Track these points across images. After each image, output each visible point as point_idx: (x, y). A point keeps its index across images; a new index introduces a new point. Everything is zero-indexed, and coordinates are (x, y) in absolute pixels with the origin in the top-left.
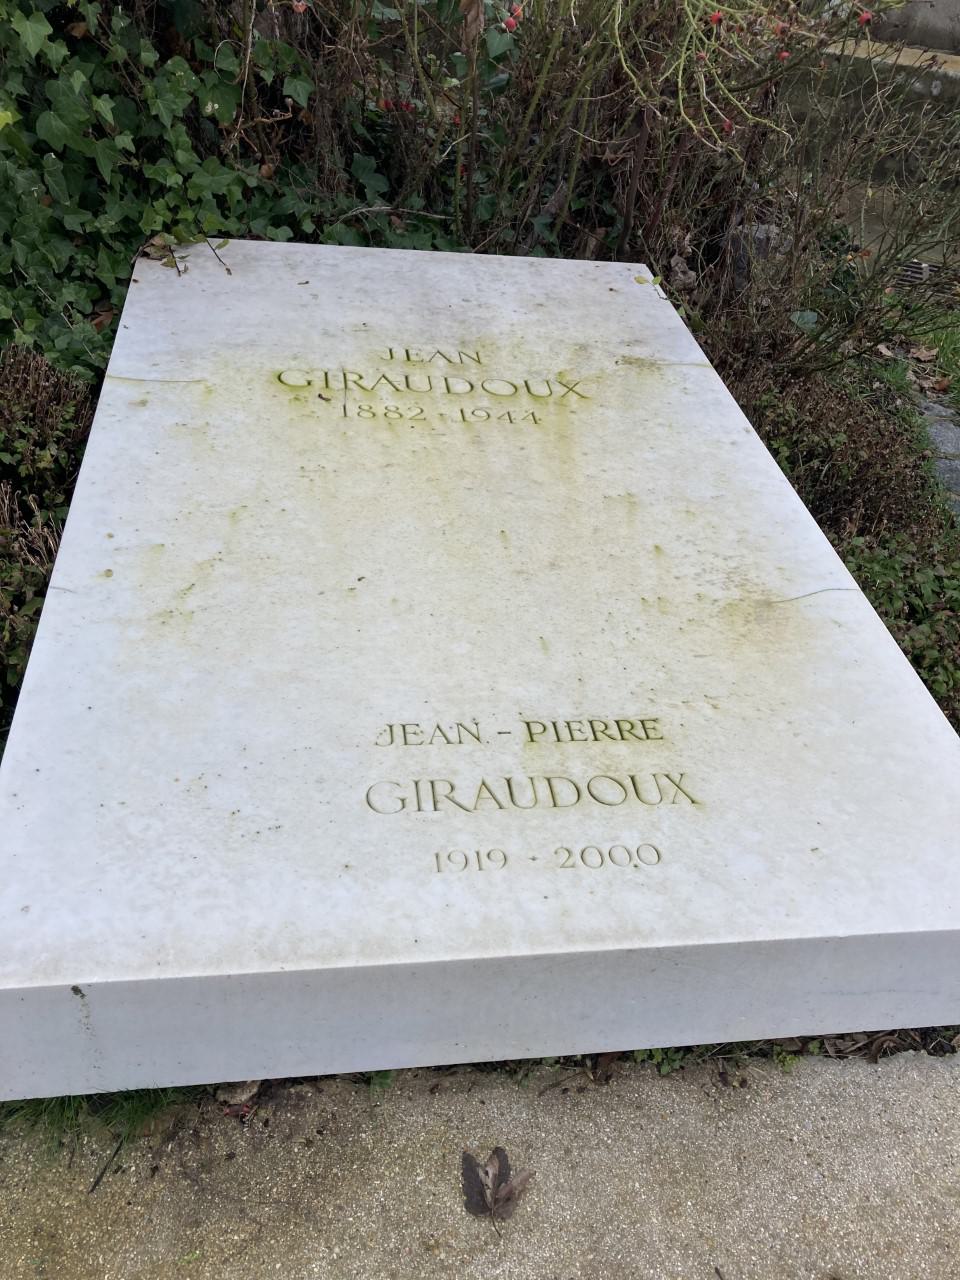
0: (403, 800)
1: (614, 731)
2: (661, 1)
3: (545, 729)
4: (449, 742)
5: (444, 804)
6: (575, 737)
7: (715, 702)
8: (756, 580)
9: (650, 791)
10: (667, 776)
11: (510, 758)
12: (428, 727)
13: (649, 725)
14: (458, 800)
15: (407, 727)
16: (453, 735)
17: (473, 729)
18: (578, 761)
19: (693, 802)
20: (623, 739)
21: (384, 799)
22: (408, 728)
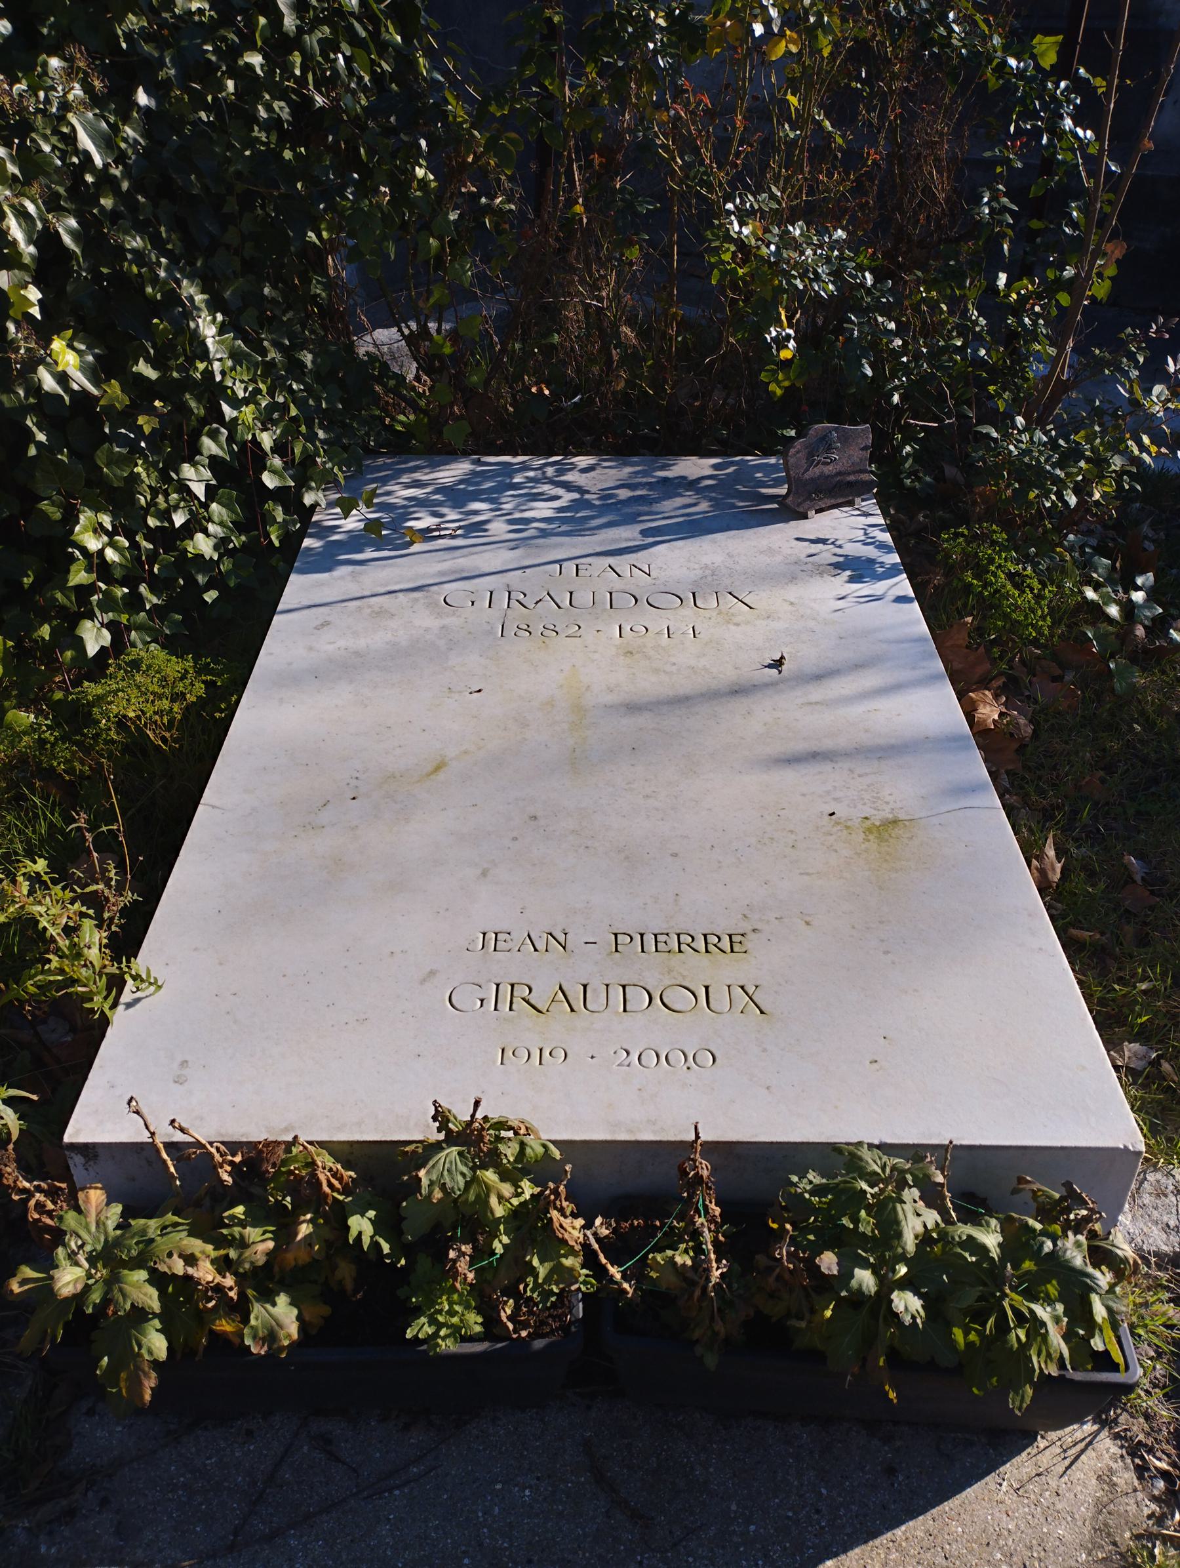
0: (482, 1001)
1: (725, 944)
2: (301, 5)
3: (632, 939)
4: (536, 950)
5: (519, 1004)
6: (735, 949)
7: (808, 919)
8: (888, 798)
9: (720, 999)
10: (742, 987)
11: (588, 966)
12: (519, 935)
13: (736, 939)
14: (532, 1001)
15: (619, 936)
16: (541, 946)
17: (561, 938)
18: (651, 970)
19: (762, 1012)
20: (707, 951)
21: (467, 998)
22: (735, 938)
